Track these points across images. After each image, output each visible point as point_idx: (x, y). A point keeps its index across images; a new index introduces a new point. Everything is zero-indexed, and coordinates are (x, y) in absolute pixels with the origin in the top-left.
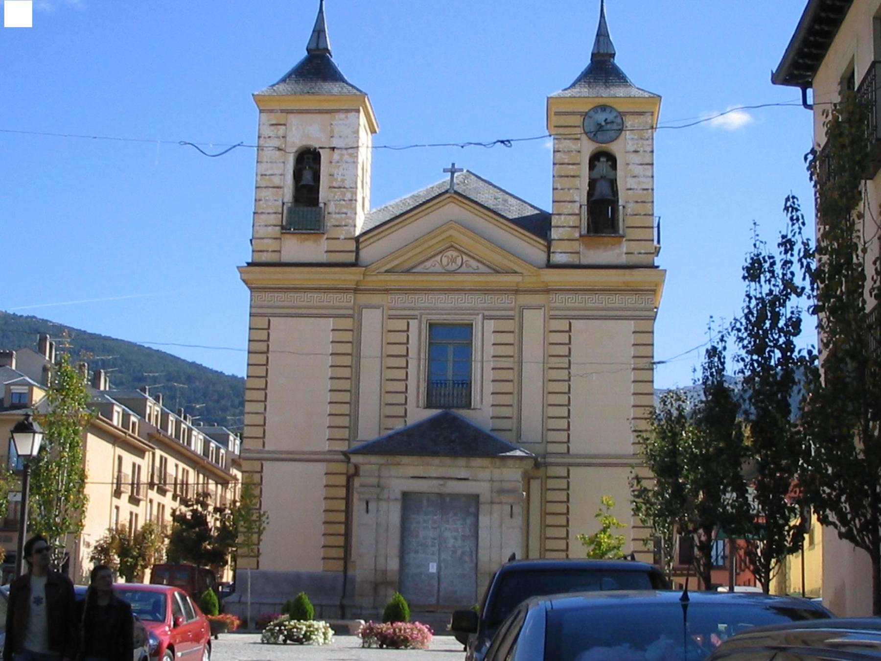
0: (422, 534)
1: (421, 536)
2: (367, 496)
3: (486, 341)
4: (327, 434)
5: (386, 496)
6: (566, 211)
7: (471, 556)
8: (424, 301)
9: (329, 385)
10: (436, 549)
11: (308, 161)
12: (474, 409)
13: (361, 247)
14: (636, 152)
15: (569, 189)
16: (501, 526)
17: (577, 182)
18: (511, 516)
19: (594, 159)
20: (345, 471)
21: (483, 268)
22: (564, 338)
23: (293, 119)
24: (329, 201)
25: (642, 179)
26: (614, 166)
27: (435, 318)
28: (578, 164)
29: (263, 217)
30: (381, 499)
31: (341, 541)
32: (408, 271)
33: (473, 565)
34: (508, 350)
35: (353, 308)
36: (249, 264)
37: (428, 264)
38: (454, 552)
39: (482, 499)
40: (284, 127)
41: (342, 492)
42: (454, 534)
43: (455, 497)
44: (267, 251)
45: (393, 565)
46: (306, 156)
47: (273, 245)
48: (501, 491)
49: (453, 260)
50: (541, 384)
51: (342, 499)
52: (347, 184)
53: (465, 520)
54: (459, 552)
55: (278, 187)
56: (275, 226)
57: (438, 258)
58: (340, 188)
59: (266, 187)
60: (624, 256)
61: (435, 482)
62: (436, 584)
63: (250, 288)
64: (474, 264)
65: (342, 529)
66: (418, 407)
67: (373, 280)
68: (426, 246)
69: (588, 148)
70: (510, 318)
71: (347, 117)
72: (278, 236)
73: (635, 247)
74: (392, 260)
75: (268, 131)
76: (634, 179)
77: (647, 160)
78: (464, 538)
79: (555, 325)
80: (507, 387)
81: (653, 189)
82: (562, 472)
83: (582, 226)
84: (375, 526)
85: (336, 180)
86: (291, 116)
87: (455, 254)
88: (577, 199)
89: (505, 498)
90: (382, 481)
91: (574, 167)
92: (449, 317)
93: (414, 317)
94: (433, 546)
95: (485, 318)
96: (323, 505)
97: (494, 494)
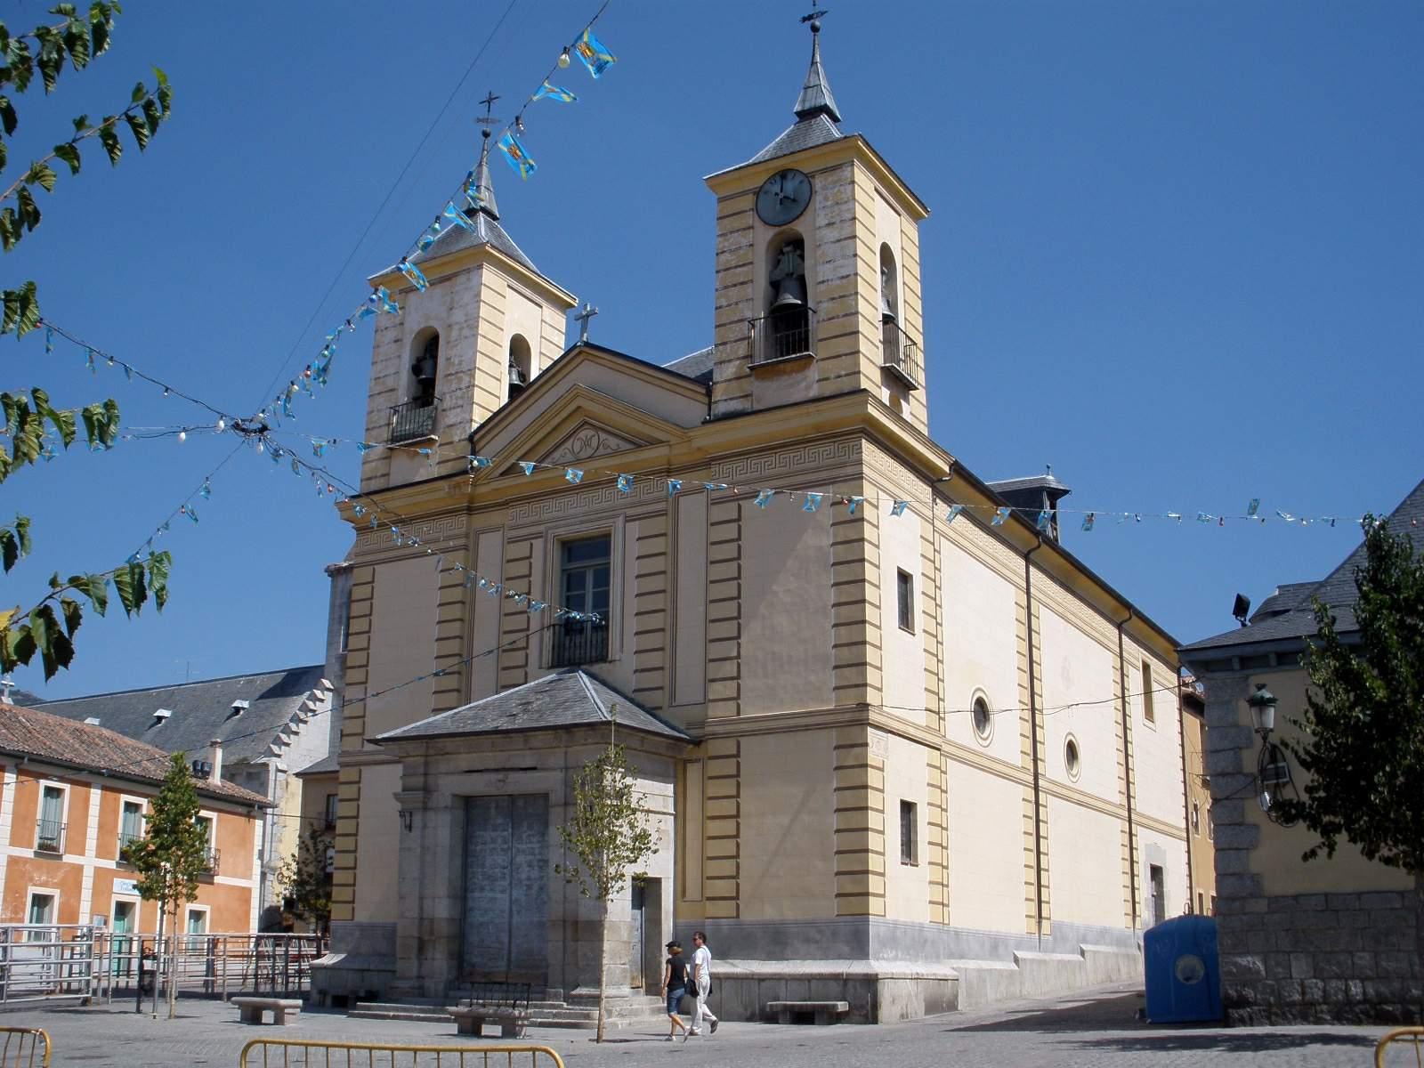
0: (489, 862)
10: (506, 883)
11: (429, 346)
14: (829, 225)
15: (737, 304)
17: (749, 289)
24: (444, 394)
25: (841, 262)
27: (566, 532)
28: (752, 263)
30: (431, 809)
35: (467, 536)
37: (557, 455)
38: (529, 887)
39: (553, 798)
44: (376, 477)
45: (442, 909)
57: (568, 444)
59: (379, 394)
60: (816, 386)
62: (506, 940)
63: (357, 529)
64: (613, 442)
66: (540, 668)
70: (663, 513)
73: (832, 367)
76: (828, 265)
77: (846, 233)
79: (720, 513)
82: (728, 747)
83: (757, 352)
84: (419, 850)
85: (453, 364)
87: (590, 432)
90: (431, 780)
91: (745, 269)
92: (583, 527)
94: (503, 878)
95: (628, 519)
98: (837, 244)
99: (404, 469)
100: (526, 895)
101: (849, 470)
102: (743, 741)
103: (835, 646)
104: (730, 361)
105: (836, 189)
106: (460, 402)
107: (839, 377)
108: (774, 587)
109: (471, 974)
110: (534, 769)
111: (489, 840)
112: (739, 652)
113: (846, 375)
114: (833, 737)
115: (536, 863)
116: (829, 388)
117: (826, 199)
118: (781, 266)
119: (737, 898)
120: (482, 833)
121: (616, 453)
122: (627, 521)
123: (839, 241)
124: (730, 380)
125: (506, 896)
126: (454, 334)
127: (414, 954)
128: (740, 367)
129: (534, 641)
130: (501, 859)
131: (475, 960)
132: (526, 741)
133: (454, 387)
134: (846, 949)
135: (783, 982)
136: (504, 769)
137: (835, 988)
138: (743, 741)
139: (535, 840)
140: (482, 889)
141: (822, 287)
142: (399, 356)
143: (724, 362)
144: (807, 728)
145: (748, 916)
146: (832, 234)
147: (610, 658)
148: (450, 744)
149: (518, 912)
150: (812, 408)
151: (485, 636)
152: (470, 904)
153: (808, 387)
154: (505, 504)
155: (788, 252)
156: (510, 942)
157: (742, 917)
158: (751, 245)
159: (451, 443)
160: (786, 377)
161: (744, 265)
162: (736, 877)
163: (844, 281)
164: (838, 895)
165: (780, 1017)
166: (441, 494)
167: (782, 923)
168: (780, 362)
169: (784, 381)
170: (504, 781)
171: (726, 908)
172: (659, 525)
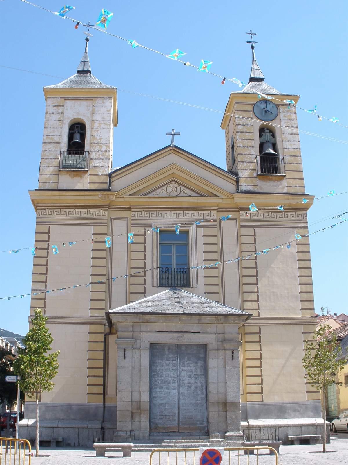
1: (164, 376)
2: (125, 346)
3: (198, 242)
4: (90, 305)
5: (138, 346)
6: (246, 160)
7: (202, 389)
8: (156, 215)
9: (91, 271)
12: (192, 287)
13: (112, 180)
15: (248, 147)
16: (225, 367)
17: (253, 143)
18: (233, 359)
19: (262, 130)
20: (103, 331)
21: (194, 194)
22: (251, 240)
23: (68, 103)
24: (91, 151)
26: (273, 136)
28: (253, 132)
29: (47, 161)
31: (100, 381)
32: (145, 195)
33: (204, 396)
34: (215, 248)
35: (107, 219)
36: (36, 190)
37: (158, 191)
38: (190, 387)
39: (210, 347)
40: (62, 107)
41: (101, 346)
42: (188, 374)
43: (188, 346)
45: (145, 397)
46: (75, 126)
47: (53, 179)
48: (224, 341)
49: (175, 189)
50: (237, 270)
51: (101, 350)
52: (103, 141)
53: (197, 363)
54: (193, 388)
55: (57, 143)
56: (56, 166)
58: (98, 143)
60: (286, 188)
61: (175, 335)
62: (177, 412)
64: (189, 192)
65: (101, 372)
66: (153, 286)
67: (120, 201)
68: (157, 179)
69: (258, 123)
71: (103, 102)
72: (58, 173)
73: (293, 183)
74: (134, 188)
75: (51, 110)
78: (197, 376)
79: (244, 231)
80: (214, 272)
81: (300, 149)
82: (256, 329)
85: (96, 139)
86: (68, 101)
88: (253, 153)
89: (227, 346)
91: (250, 134)
93: (150, 226)
94: (174, 383)
95: (197, 226)
96: (88, 355)
97: (220, 343)
98: (291, 135)
99: (65, 181)
100: (188, 391)
101: (302, 224)
102: (262, 327)
103: (300, 292)
104: (247, 170)
105: (289, 114)
106: (101, 157)
107: (296, 187)
108: (272, 266)
109: (156, 428)
110: (199, 332)
111: (165, 364)
112: (258, 290)
113: (299, 187)
114: (302, 329)
115: (193, 376)
116: (292, 191)
117: (285, 116)
118: (104, 127)
119: (262, 393)
120: (159, 361)
121: (190, 197)
122: (197, 227)
123: (291, 134)
124: (247, 177)
125: (176, 391)
126: (96, 125)
127: (129, 419)
128: (251, 173)
129: (149, 274)
130: (172, 374)
131: (157, 421)
132: (199, 319)
133: (97, 149)
134: (311, 414)
135: (290, 428)
136: (181, 332)
137: (312, 429)
138: (262, 327)
139: (192, 365)
140: (161, 388)
141: (286, 150)
142: (62, 128)
143: (243, 169)
144: (291, 324)
145: (268, 400)
146: (289, 130)
147: (191, 286)
148: (153, 317)
149: (184, 399)
150: (287, 196)
151: (119, 269)
152: (154, 394)
153: (283, 188)
154: (130, 209)
155: (267, 132)
156: (179, 412)
157: (264, 401)
158: (252, 125)
159: (97, 175)
160: (272, 182)
161: (250, 132)
162: (262, 384)
163: (295, 150)
164: (307, 392)
165: (295, 442)
166: (97, 198)
167: (283, 403)
168: (271, 175)
169: (272, 183)
170: (181, 337)
171: (258, 397)
172: (214, 231)
